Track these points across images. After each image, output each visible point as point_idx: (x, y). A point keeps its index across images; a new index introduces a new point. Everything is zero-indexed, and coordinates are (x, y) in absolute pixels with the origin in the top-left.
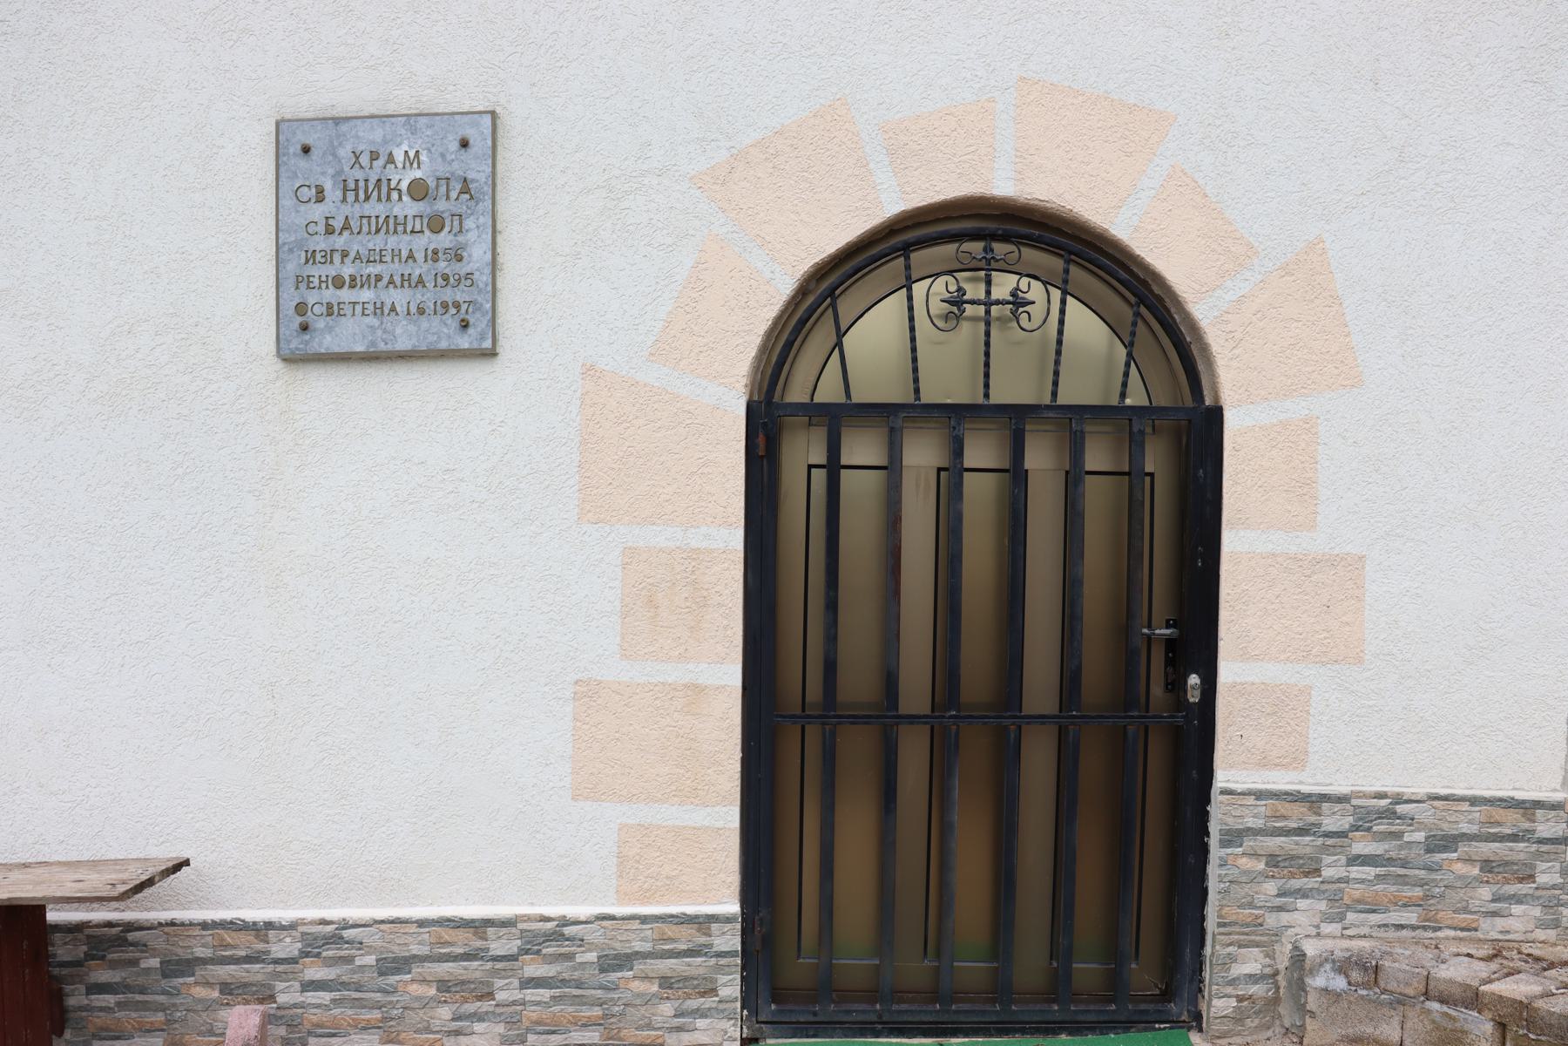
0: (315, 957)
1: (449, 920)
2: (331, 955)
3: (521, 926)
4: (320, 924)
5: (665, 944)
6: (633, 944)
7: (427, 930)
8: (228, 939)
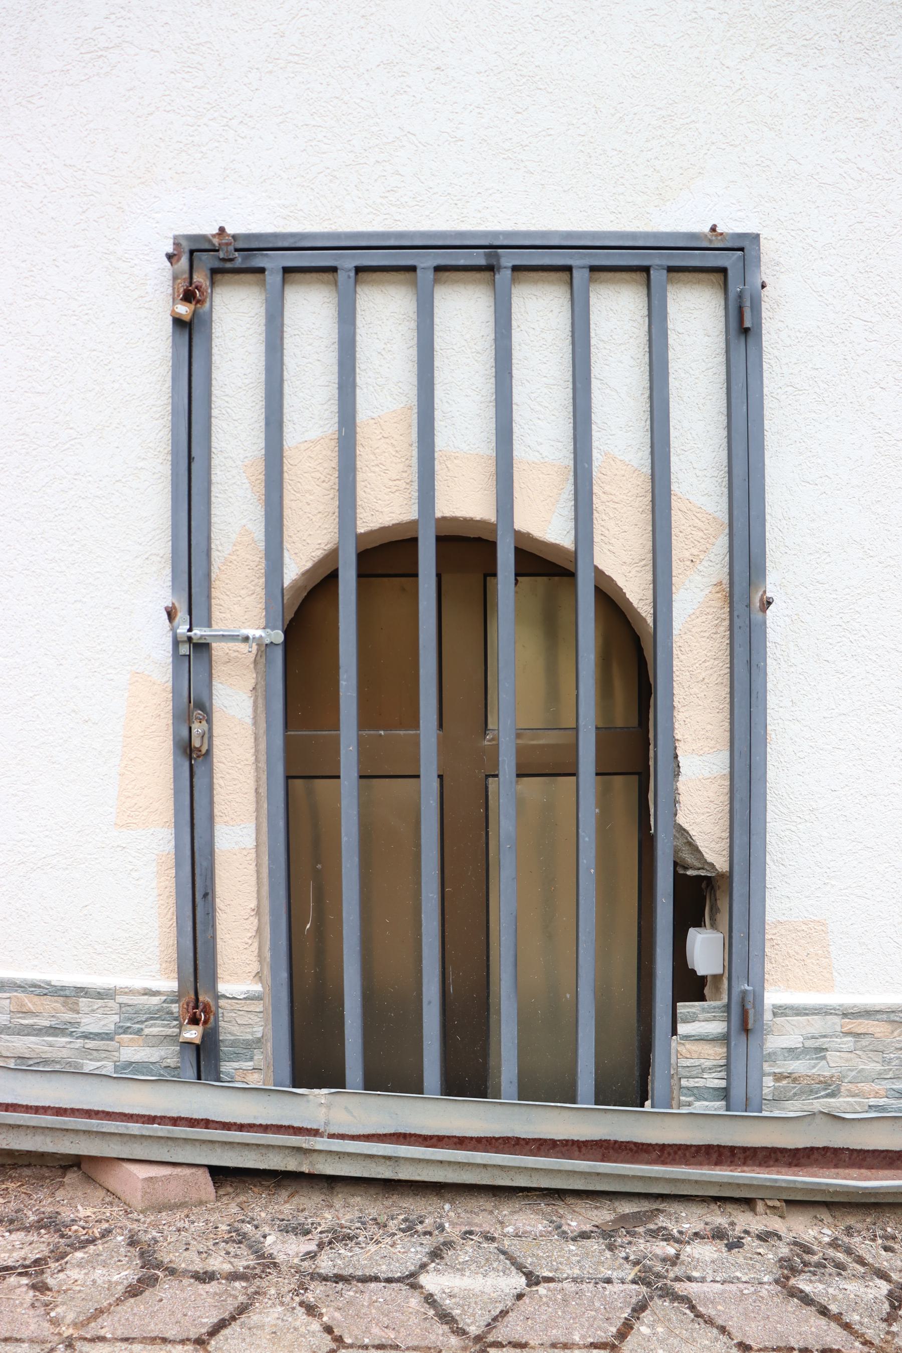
0: (135, 1034)
1: (34, 986)
2: (153, 1033)
3: (121, 999)
4: (145, 994)
5: (24, 1018)
6: (254, 1030)
7: (8, 995)
8: (29, 1005)
